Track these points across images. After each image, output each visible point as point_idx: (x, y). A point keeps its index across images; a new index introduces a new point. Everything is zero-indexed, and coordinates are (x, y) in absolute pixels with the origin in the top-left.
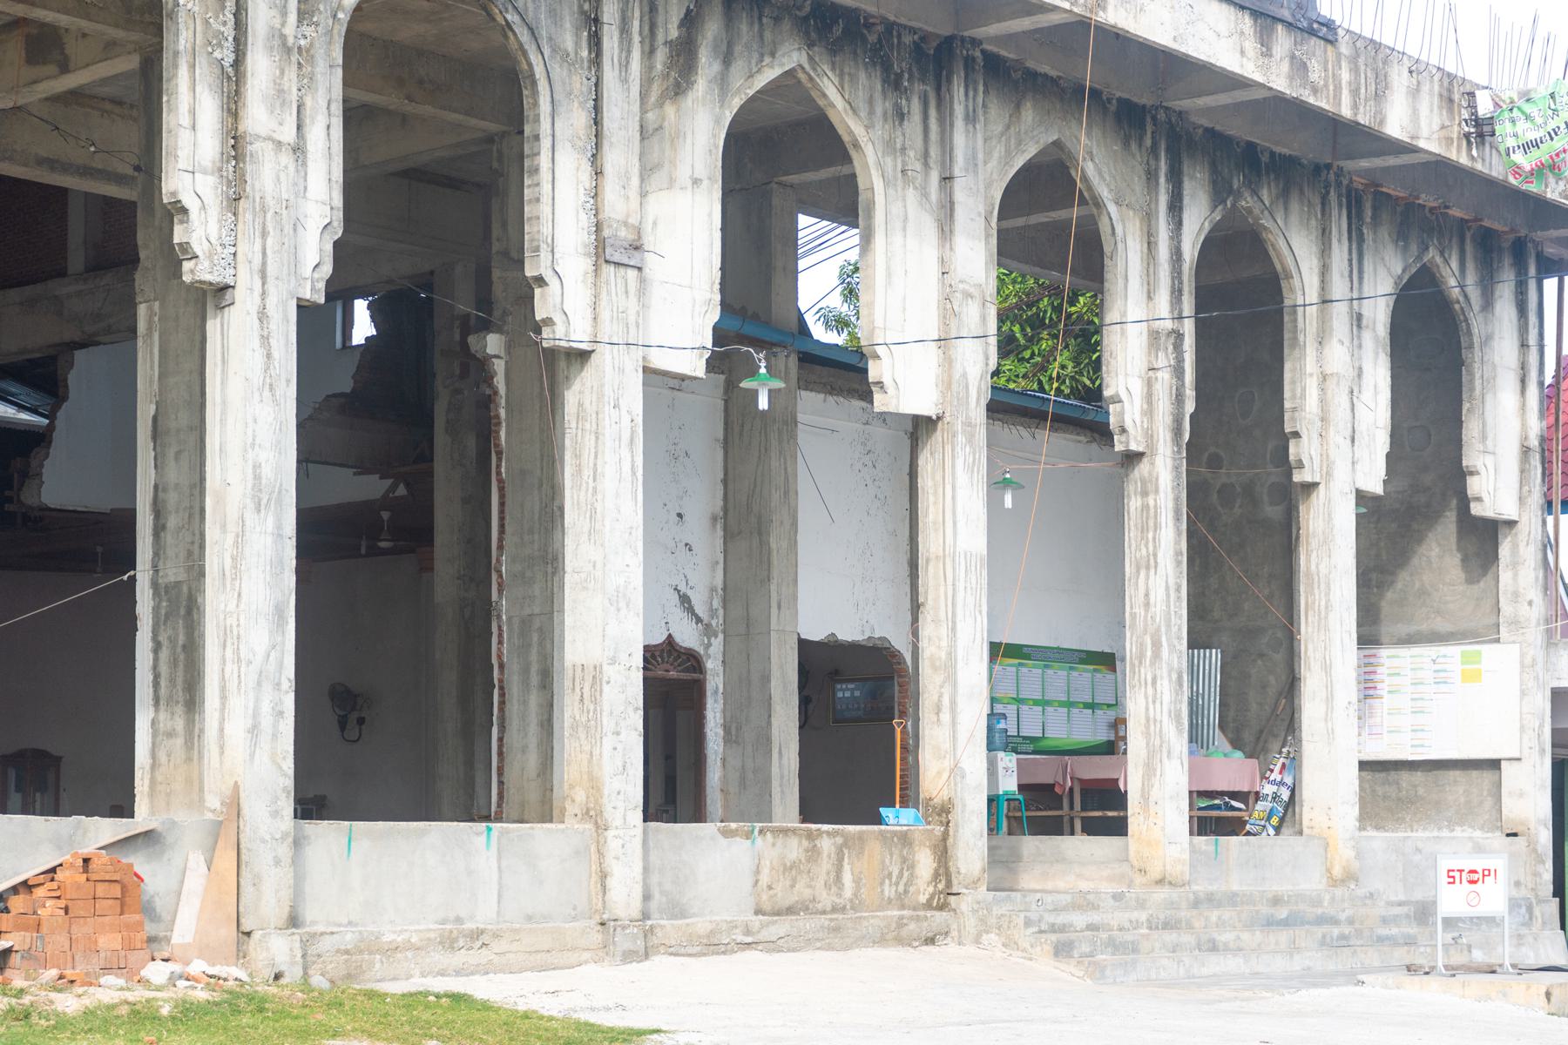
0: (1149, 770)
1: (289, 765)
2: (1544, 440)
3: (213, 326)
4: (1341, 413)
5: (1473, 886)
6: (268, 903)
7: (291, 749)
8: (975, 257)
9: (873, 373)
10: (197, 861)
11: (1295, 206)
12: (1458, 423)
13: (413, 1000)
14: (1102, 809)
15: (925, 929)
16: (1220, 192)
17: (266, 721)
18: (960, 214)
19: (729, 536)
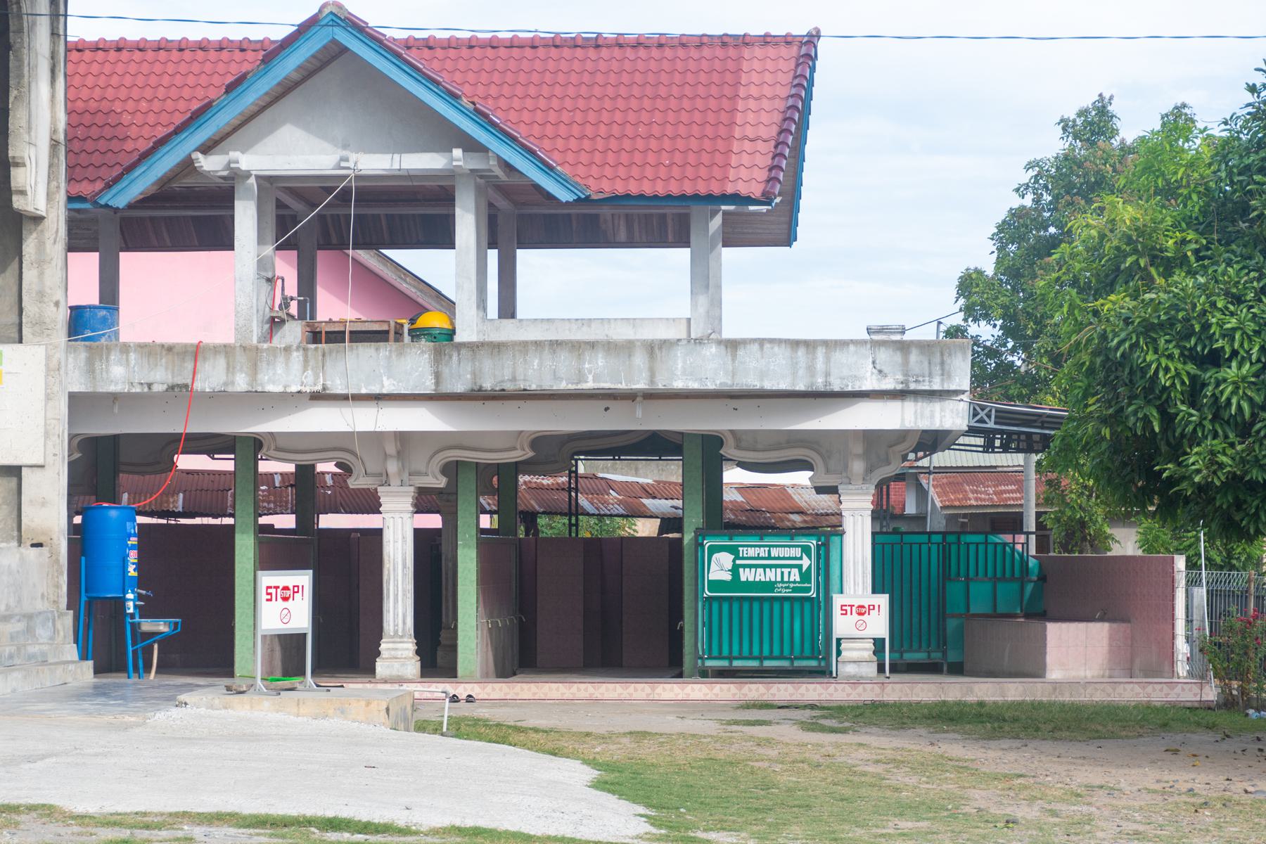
5: (286, 604)
7: (237, 597)
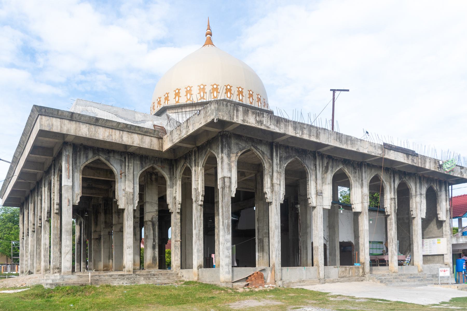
0: (392, 257)
1: (280, 260)
2: (450, 209)
3: (270, 207)
4: (419, 207)
6: (278, 277)
8: (366, 190)
9: (352, 206)
10: (270, 272)
11: (411, 179)
12: (436, 207)
13: (297, 289)
14: (384, 263)
15: (361, 279)
16: (400, 178)
17: (278, 255)
18: (364, 185)
19: (329, 229)
